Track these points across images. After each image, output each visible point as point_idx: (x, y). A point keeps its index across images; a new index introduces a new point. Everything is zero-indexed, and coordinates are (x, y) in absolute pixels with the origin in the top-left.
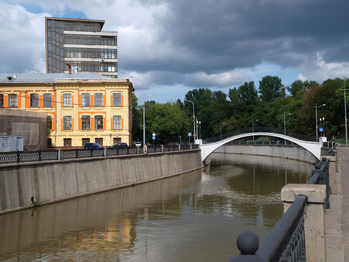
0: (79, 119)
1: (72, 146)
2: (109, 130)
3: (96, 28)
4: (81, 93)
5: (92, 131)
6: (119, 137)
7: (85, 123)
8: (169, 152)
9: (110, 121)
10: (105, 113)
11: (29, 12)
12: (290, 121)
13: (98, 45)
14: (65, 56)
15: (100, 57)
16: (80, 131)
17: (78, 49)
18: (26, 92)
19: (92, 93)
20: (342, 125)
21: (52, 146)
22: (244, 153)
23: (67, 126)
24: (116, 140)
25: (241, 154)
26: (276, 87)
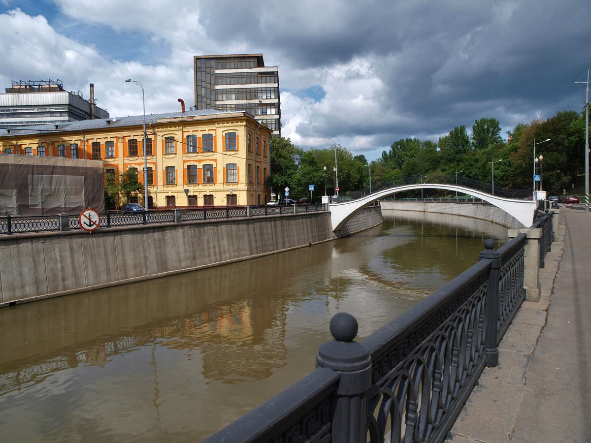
0: (184, 169)
1: (176, 205)
2: (221, 183)
3: (252, 64)
4: (186, 135)
5: (200, 185)
6: (234, 193)
7: (191, 174)
8: (308, 213)
9: (222, 172)
10: (215, 160)
11: (117, 28)
12: (502, 170)
13: (255, 83)
14: (217, 99)
15: (257, 98)
16: (185, 186)
17: (232, 90)
18: (124, 137)
19: (199, 134)
20: (579, 174)
21: (154, 206)
22: (445, 212)
23: (170, 181)
24: (230, 197)
25: (442, 213)
26: (493, 132)
